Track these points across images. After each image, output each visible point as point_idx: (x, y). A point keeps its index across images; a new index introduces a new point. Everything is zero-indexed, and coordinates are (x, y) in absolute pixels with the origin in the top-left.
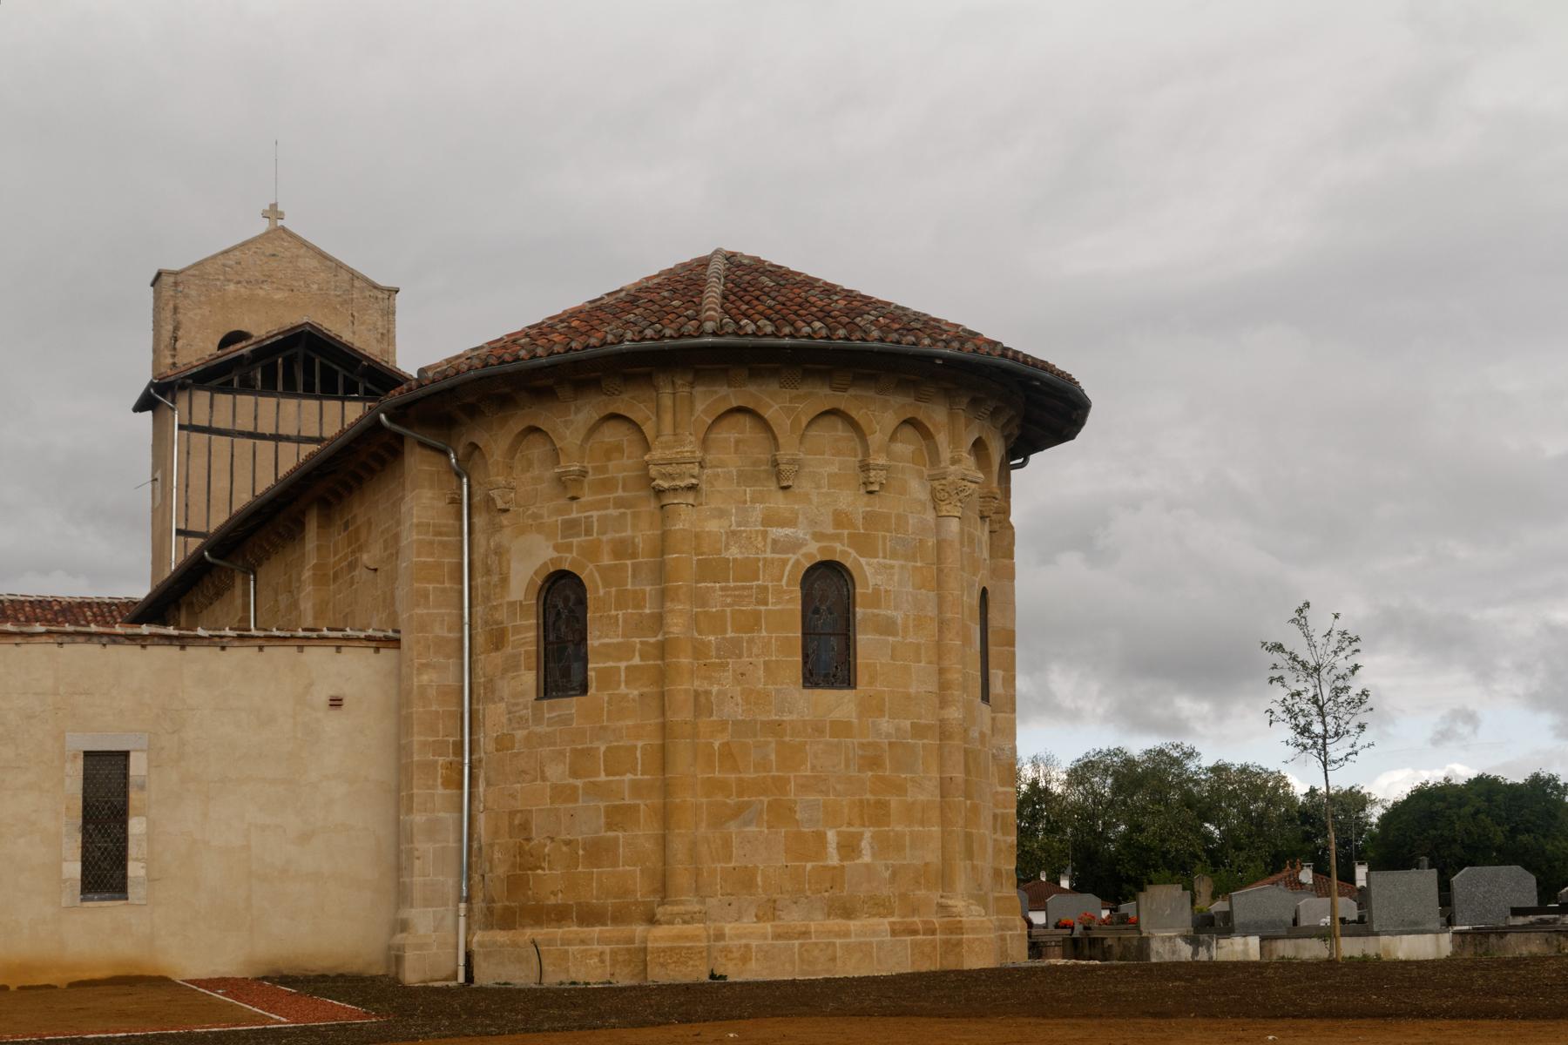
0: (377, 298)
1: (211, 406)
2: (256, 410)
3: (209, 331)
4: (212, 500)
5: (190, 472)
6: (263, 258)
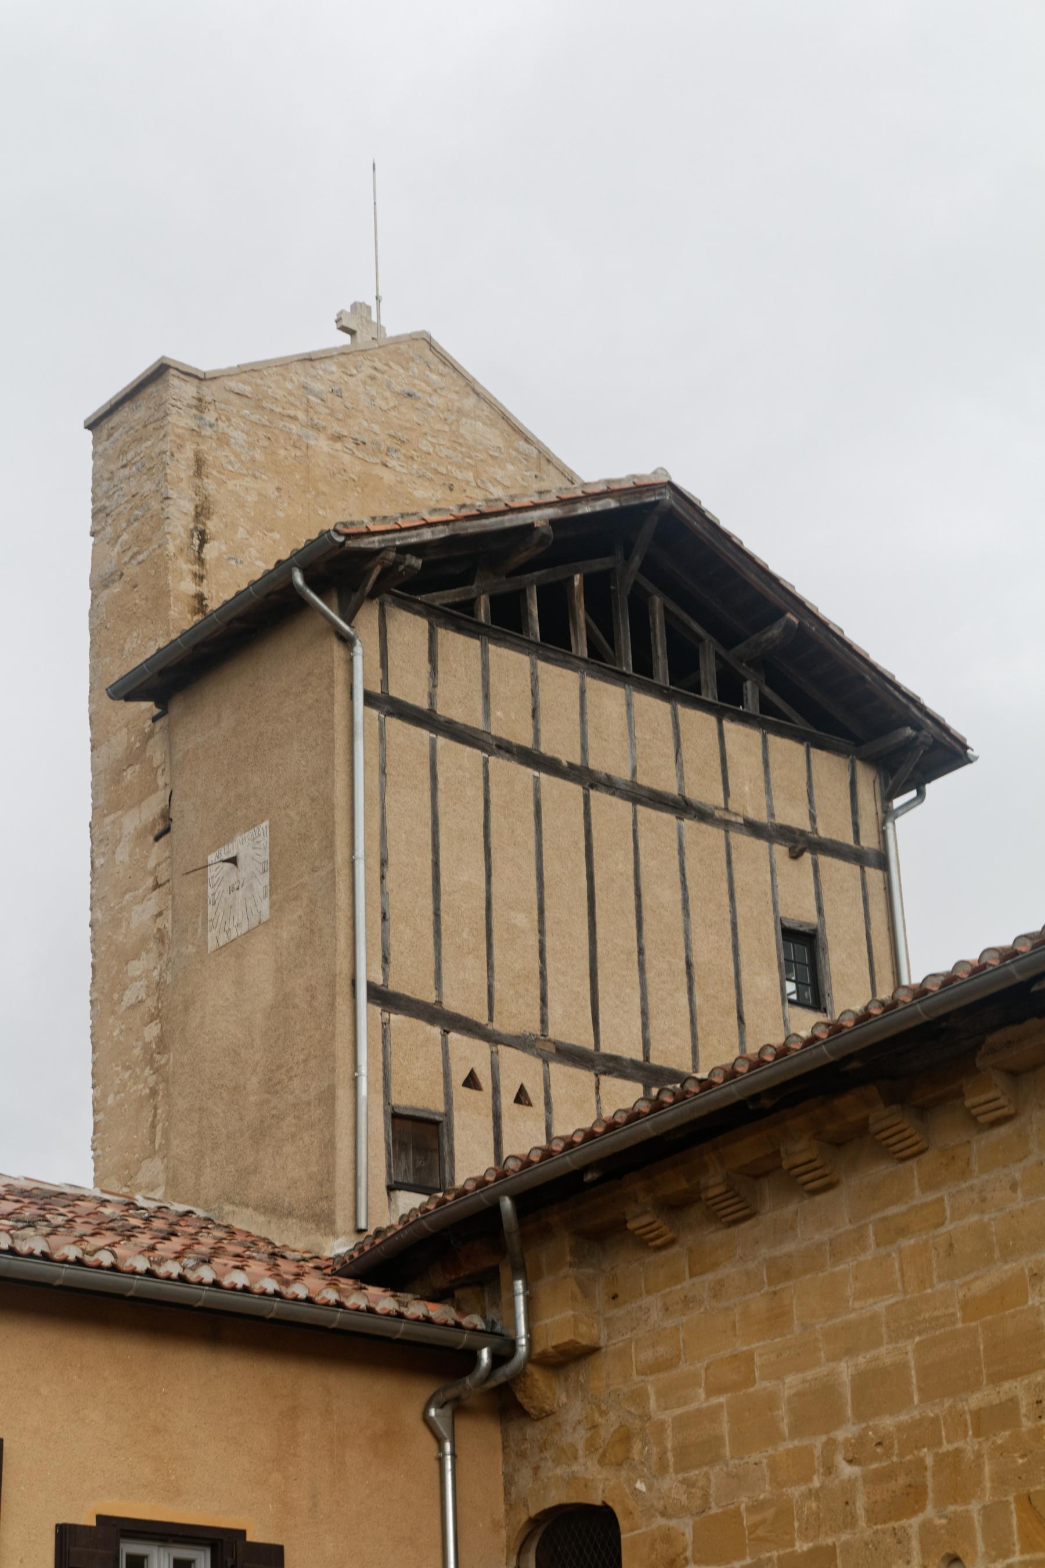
1: (433, 659)
2: (534, 693)
3: (276, 536)
4: (445, 917)
5: (389, 826)
6: (388, 394)
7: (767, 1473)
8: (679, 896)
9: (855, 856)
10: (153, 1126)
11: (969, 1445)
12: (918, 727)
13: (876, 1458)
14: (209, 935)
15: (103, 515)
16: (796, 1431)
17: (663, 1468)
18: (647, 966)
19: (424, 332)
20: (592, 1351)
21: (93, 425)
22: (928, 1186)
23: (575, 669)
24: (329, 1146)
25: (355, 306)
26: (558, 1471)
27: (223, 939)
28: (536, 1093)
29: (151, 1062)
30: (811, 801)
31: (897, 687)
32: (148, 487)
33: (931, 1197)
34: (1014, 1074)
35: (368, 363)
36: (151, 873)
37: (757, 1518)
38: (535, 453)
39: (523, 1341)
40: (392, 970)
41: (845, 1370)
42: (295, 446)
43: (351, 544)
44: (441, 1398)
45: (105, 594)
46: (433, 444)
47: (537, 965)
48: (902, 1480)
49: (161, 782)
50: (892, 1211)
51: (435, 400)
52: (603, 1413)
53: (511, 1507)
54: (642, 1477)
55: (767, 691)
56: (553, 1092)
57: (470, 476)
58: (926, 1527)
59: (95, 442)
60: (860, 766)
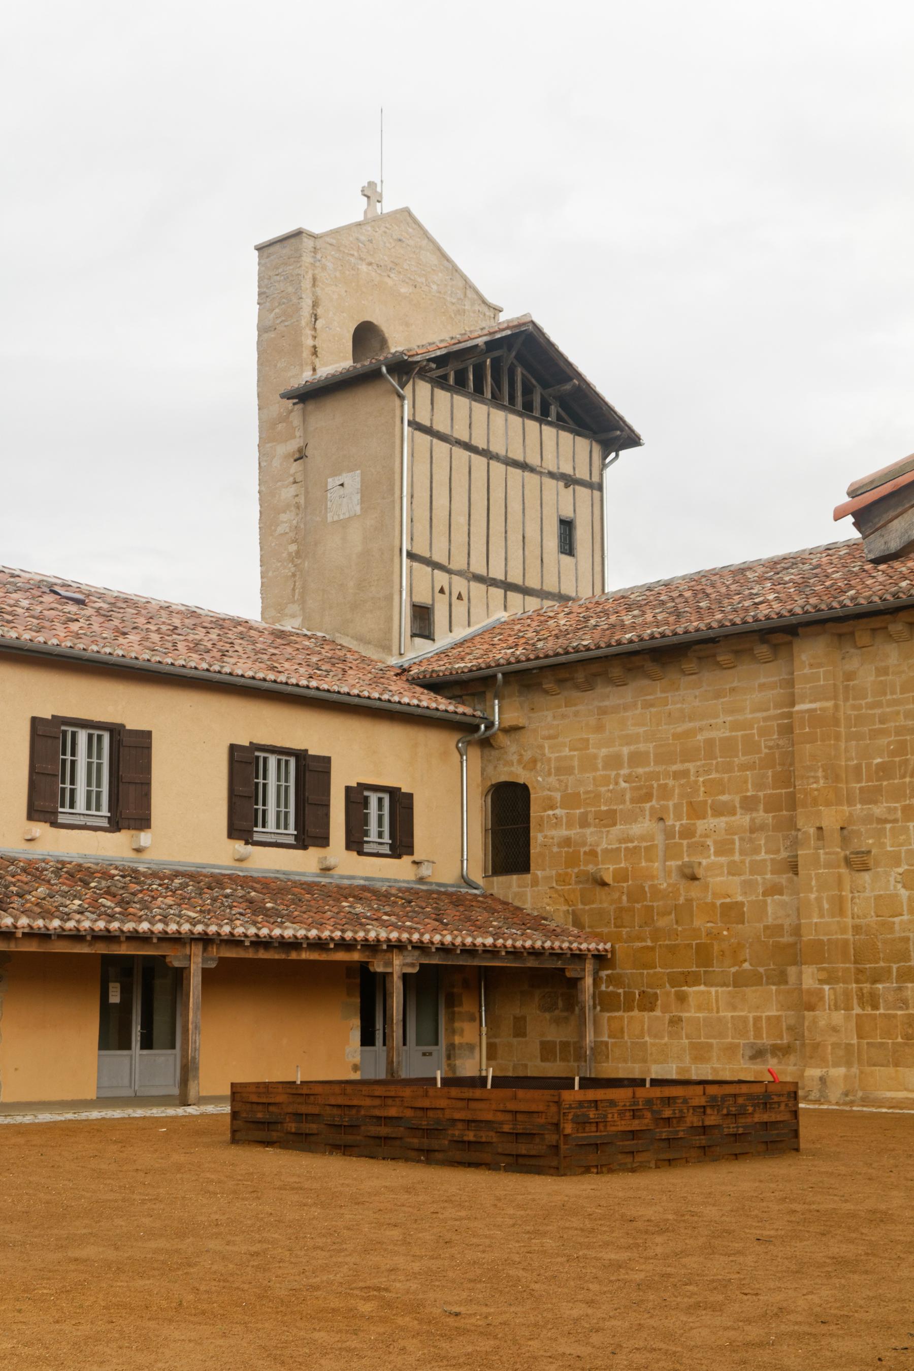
0: (485, 315)
2: (470, 417)
3: (345, 315)
7: (592, 781)
8: (522, 507)
9: (589, 485)
10: (294, 590)
11: (671, 782)
12: (622, 431)
13: (634, 782)
14: (328, 515)
15: (265, 296)
16: (604, 768)
17: (550, 774)
18: (508, 538)
19: (407, 208)
20: (523, 728)
21: (260, 249)
22: (663, 691)
23: (486, 404)
24: (390, 619)
25: (369, 183)
26: (505, 769)
27: (336, 518)
28: (465, 596)
29: (292, 561)
30: (574, 461)
31: (615, 413)
32: (290, 289)
33: (664, 695)
34: (700, 658)
35: (383, 225)
36: (292, 475)
37: (587, 796)
38: (451, 267)
39: (497, 723)
40: (414, 544)
41: (625, 750)
42: (352, 269)
43: (410, 359)
44: (464, 740)
45: (266, 336)
46: (409, 265)
47: (467, 539)
48: (644, 791)
49: (298, 434)
50: (648, 697)
51: (411, 242)
52: (525, 751)
53: (483, 779)
54: (541, 776)
55: (560, 410)
56: (471, 595)
57: (423, 280)
58: (652, 808)
59: (260, 257)
60: (594, 444)
